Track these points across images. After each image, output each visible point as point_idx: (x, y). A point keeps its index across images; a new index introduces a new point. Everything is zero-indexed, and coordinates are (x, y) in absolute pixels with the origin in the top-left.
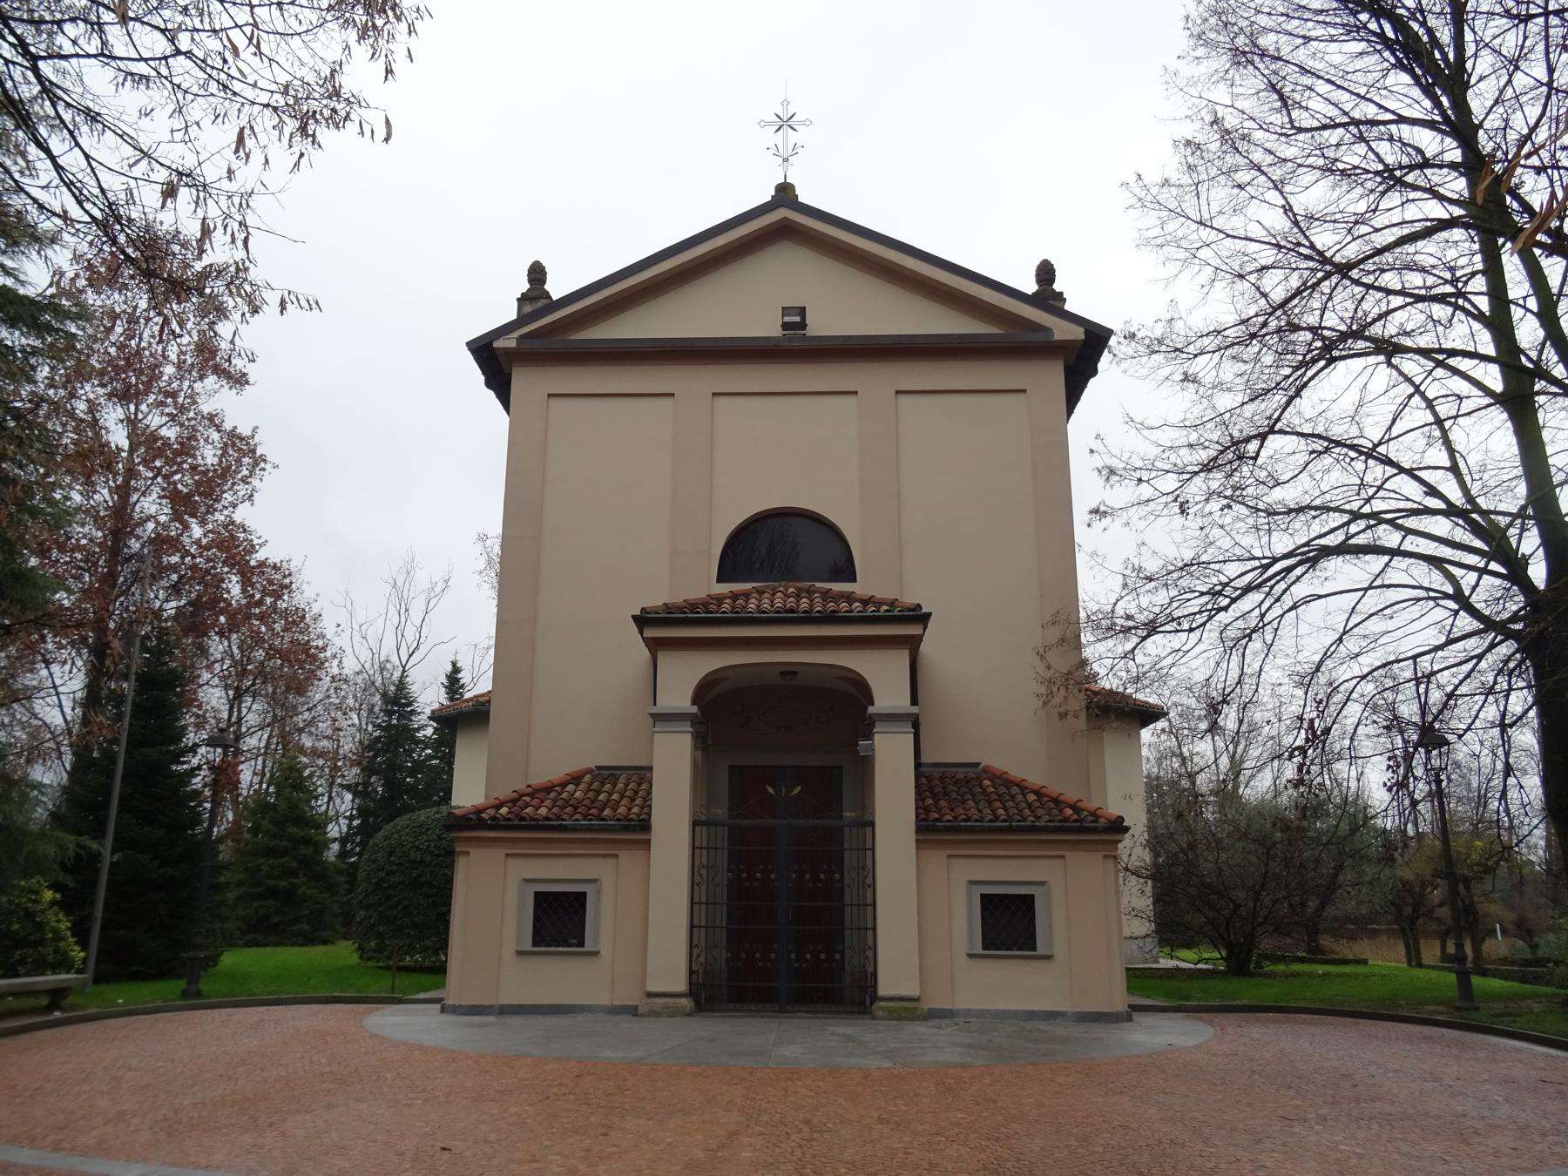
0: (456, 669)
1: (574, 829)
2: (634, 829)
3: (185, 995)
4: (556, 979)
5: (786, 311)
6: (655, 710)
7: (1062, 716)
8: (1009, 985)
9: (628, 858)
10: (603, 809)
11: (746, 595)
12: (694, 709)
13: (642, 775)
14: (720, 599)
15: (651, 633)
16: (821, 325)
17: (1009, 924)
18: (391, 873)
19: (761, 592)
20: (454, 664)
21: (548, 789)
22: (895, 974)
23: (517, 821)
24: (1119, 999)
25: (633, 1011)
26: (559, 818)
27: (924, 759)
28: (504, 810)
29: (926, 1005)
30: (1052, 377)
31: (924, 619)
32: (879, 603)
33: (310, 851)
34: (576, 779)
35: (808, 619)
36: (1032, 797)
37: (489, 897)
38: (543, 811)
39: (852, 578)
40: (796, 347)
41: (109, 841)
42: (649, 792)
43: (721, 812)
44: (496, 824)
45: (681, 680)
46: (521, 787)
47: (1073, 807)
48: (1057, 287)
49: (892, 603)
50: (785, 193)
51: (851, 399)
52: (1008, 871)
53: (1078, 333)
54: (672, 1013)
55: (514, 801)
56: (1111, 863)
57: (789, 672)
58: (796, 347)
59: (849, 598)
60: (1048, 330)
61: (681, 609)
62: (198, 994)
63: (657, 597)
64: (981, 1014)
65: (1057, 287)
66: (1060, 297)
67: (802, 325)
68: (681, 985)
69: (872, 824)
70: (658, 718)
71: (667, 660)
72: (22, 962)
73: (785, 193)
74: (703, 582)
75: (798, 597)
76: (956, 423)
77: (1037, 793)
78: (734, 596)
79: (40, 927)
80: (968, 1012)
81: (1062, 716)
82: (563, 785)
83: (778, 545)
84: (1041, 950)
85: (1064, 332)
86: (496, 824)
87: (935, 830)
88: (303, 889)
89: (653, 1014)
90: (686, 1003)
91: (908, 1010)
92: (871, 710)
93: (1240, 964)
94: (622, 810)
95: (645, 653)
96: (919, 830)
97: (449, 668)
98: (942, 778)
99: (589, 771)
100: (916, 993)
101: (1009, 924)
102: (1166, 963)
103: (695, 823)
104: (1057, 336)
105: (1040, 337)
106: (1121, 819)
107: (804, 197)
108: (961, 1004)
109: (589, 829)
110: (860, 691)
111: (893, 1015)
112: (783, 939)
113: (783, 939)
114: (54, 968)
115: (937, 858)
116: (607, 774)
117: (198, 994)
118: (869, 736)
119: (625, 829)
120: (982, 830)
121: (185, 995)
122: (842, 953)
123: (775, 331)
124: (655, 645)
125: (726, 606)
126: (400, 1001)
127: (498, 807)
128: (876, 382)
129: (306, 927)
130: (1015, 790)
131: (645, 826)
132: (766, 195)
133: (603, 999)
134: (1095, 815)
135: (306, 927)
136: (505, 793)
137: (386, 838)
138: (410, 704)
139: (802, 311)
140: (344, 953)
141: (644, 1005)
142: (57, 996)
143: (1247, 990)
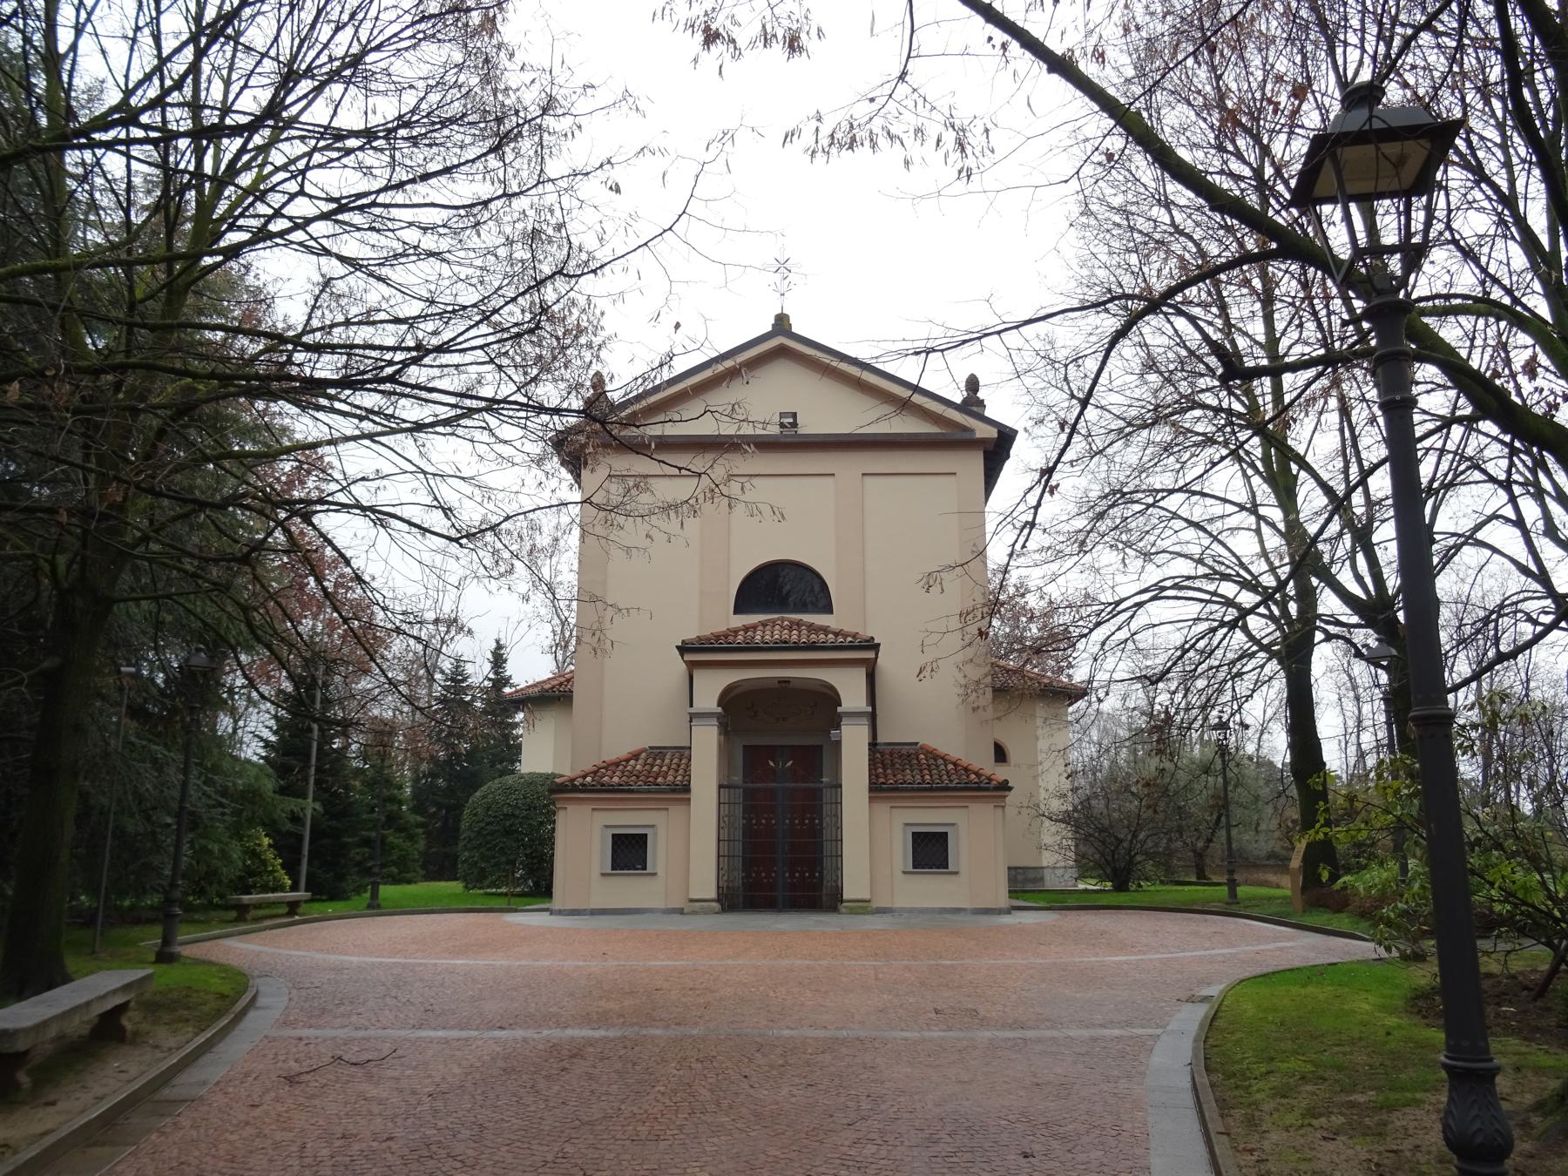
0: (499, 647)
1: (638, 792)
2: (680, 791)
3: (370, 906)
4: (629, 890)
5: (782, 415)
6: (692, 710)
7: (974, 710)
8: (930, 891)
9: (676, 811)
10: (655, 776)
11: (754, 627)
12: (720, 710)
13: (683, 753)
14: (736, 632)
15: (688, 657)
16: (810, 425)
17: (930, 851)
18: (488, 824)
19: (764, 624)
20: (498, 642)
21: (617, 764)
22: (854, 885)
23: (599, 786)
24: (1003, 900)
25: (681, 911)
26: (627, 784)
27: (880, 740)
28: (589, 779)
29: (874, 905)
30: (975, 464)
31: (876, 647)
32: (846, 636)
33: (395, 807)
34: (636, 756)
35: (797, 647)
36: (951, 766)
37: (580, 839)
38: (616, 779)
39: (828, 609)
40: (789, 441)
41: (310, 800)
42: (688, 765)
43: (737, 779)
44: (584, 789)
45: (710, 688)
46: (598, 763)
47: (976, 773)
48: (980, 395)
49: (855, 636)
50: (782, 322)
51: (829, 480)
52: (930, 816)
53: (993, 433)
54: (706, 912)
55: (595, 773)
56: (1000, 811)
57: (785, 681)
58: (789, 441)
59: (826, 630)
60: (972, 431)
61: (708, 640)
62: (379, 906)
63: (691, 634)
64: (911, 910)
65: (980, 395)
66: (981, 403)
67: (794, 425)
68: (713, 894)
69: (841, 786)
70: (692, 717)
71: (700, 677)
72: (254, 886)
73: (782, 322)
74: (725, 619)
75: (790, 629)
76: (908, 499)
77: (955, 764)
78: (746, 629)
79: (264, 863)
80: (902, 910)
81: (974, 710)
82: (628, 760)
83: (779, 587)
84: (951, 868)
85: (985, 432)
86: (584, 789)
87: (882, 790)
88: (391, 839)
89: (694, 913)
90: (716, 905)
91: (862, 907)
92: (839, 709)
93: (1121, 887)
94: (670, 778)
95: (678, 665)
96: (871, 790)
97: (494, 645)
98: (891, 754)
99: (644, 750)
100: (867, 897)
101: (930, 851)
102: (1081, 886)
103: (720, 787)
104: (978, 435)
105: (967, 436)
106: (1007, 782)
107: (797, 328)
108: (897, 905)
109: (649, 792)
110: (829, 697)
111: (852, 912)
112: (781, 864)
113: (781, 864)
114: (274, 890)
115: (883, 808)
116: (657, 752)
117: (379, 906)
118: (838, 727)
119: (673, 791)
120: (913, 790)
121: (370, 906)
122: (821, 873)
123: (774, 430)
124: (692, 666)
125: (740, 638)
126: (516, 911)
127: (584, 777)
128: (848, 466)
129: (394, 870)
130: (940, 761)
131: (686, 789)
132: (767, 327)
133: (660, 905)
134: (990, 779)
135: (394, 870)
136: (588, 767)
137: (484, 797)
138: (465, 680)
139: (794, 415)
140: (456, 887)
141: (688, 907)
142: (293, 907)
143: (1122, 898)
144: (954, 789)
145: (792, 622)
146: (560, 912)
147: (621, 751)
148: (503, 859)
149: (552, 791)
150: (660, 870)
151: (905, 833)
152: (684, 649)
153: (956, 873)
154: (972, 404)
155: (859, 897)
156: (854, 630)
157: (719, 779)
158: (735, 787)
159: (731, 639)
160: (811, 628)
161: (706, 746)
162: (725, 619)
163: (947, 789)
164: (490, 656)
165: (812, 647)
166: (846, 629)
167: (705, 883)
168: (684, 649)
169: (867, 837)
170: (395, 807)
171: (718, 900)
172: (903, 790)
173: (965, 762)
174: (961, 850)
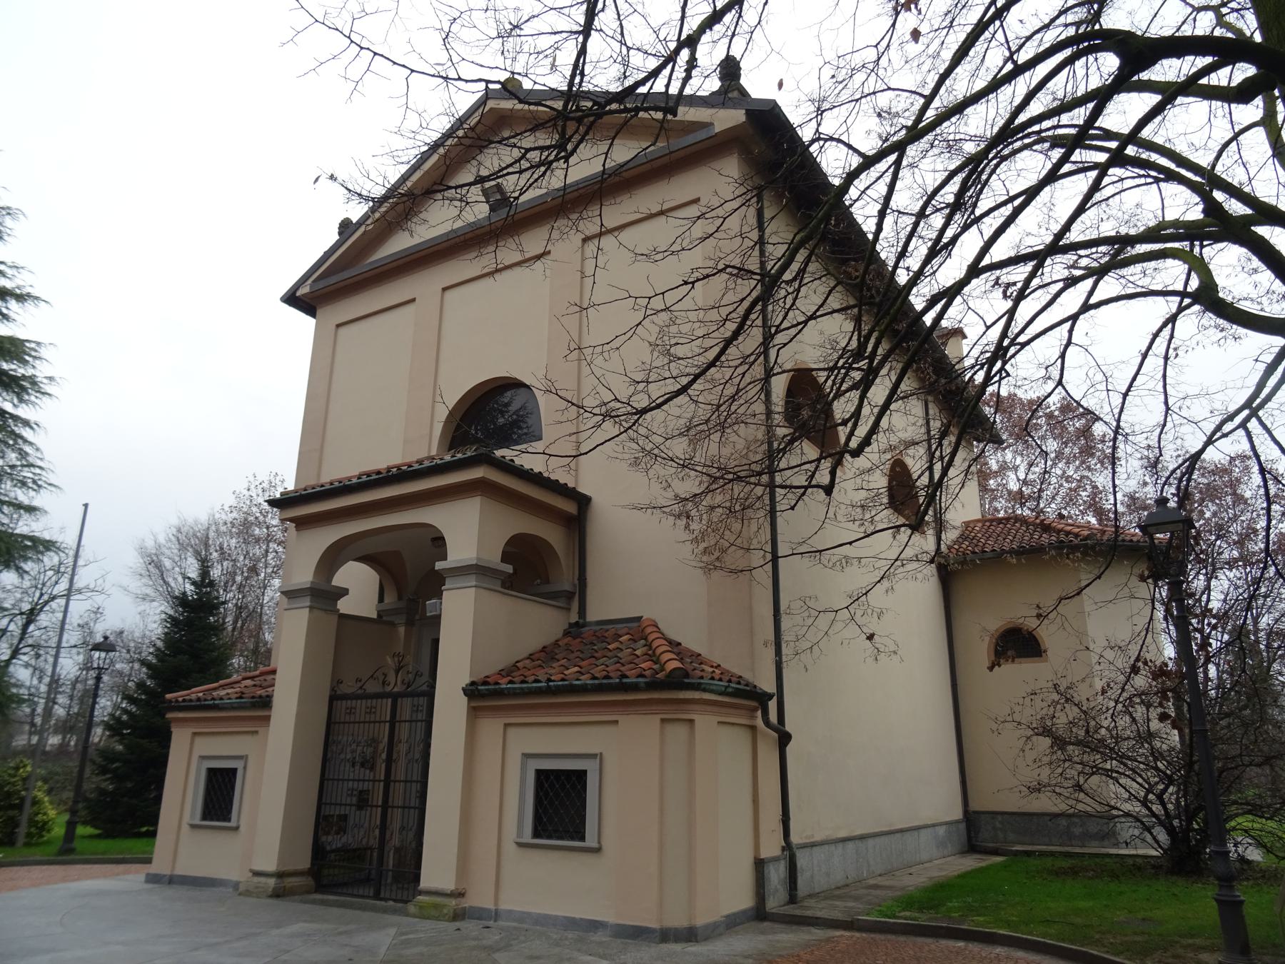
101: (560, 806)
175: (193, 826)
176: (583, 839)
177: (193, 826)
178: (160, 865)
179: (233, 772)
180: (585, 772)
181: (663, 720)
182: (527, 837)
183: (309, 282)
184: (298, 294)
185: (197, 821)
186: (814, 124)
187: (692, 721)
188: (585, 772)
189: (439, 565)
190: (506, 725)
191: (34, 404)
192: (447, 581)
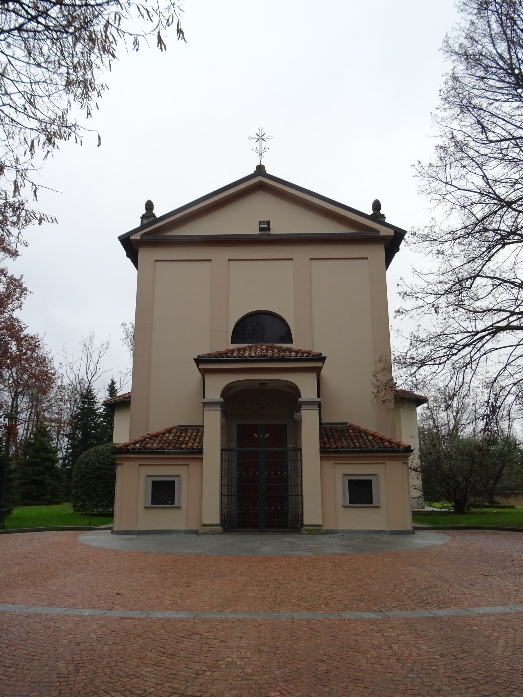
1: (169, 453)
4: (163, 518)
5: (261, 223)
7: (384, 402)
8: (360, 519)
9: (193, 466)
10: (183, 444)
11: (244, 349)
12: (222, 400)
14: (232, 351)
16: (276, 229)
17: (361, 493)
18: (87, 473)
19: (250, 348)
20: (112, 380)
21: (157, 436)
22: (311, 515)
23: (143, 450)
24: (408, 524)
25: (196, 532)
26: (162, 448)
27: (323, 421)
28: (138, 445)
29: (326, 527)
30: (380, 252)
31: (322, 359)
32: (303, 353)
34: (169, 431)
35: (272, 360)
36: (370, 437)
37: (132, 483)
38: (155, 445)
42: (202, 436)
43: (234, 445)
44: (134, 451)
45: (215, 388)
46: (145, 435)
49: (309, 353)
50: (260, 169)
52: (360, 470)
53: (391, 233)
54: (213, 533)
55: (142, 441)
57: (263, 383)
59: (290, 350)
60: (378, 231)
61: (215, 356)
63: (204, 351)
64: (349, 532)
65: (382, 212)
66: (383, 216)
67: (268, 229)
68: (217, 521)
69: (300, 450)
70: (205, 404)
71: (210, 379)
73: (260, 169)
74: (224, 344)
75: (267, 350)
76: (335, 273)
77: (373, 436)
78: (239, 350)
81: (384, 402)
82: (164, 434)
83: (259, 328)
84: (375, 504)
86: (134, 451)
87: (328, 452)
88: (47, 480)
89: (206, 533)
90: (219, 528)
91: (317, 530)
94: (190, 444)
96: (321, 452)
97: (110, 382)
98: (331, 430)
99: (175, 427)
100: (320, 522)
101: (361, 493)
102: (427, 509)
103: (222, 450)
104: (382, 234)
105: (374, 234)
106: (410, 447)
108: (339, 528)
109: (176, 453)
110: (295, 391)
111: (310, 533)
112: (262, 500)
113: (262, 500)
115: (329, 464)
116: (183, 429)
118: (299, 411)
119: (192, 453)
124: (204, 372)
125: (235, 354)
126: (93, 529)
127: (135, 444)
128: (302, 254)
129: (49, 497)
130: (363, 434)
131: (200, 451)
132: (252, 170)
133: (183, 528)
136: (138, 437)
137: (85, 458)
139: (268, 223)
141: (201, 530)
143: (463, 520)
144: (376, 452)
145: (267, 347)
146: (118, 533)
147: (160, 429)
148: (95, 494)
149: (114, 453)
150: (183, 505)
151: (343, 480)
152: (199, 361)
153: (378, 507)
154: (377, 215)
155: (315, 523)
156: (308, 349)
157: (222, 446)
158: (232, 450)
159: (229, 355)
160: (280, 349)
161: (213, 424)
162: (224, 344)
163: (372, 451)
164: (108, 388)
165: (282, 360)
166: (303, 349)
167: (212, 514)
168: (199, 361)
169: (319, 486)
170: (50, 464)
171: (222, 524)
172: (344, 452)
173: (380, 434)
174: (381, 491)
175: (146, 508)
176: (372, 503)
177: (146, 508)
178: (118, 523)
179: (173, 482)
180: (371, 480)
181: (334, 463)
182: (347, 503)
183: (140, 233)
184: (131, 238)
185: (150, 505)
186: (450, 250)
187: (188, 465)
188: (371, 480)
189: (300, 400)
190: (140, 465)
191: (158, 46)
192: (303, 406)
